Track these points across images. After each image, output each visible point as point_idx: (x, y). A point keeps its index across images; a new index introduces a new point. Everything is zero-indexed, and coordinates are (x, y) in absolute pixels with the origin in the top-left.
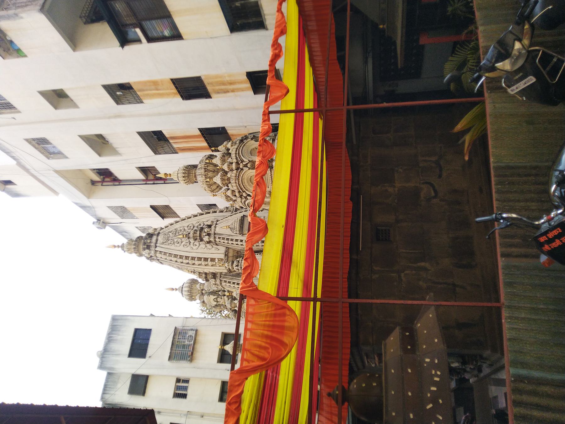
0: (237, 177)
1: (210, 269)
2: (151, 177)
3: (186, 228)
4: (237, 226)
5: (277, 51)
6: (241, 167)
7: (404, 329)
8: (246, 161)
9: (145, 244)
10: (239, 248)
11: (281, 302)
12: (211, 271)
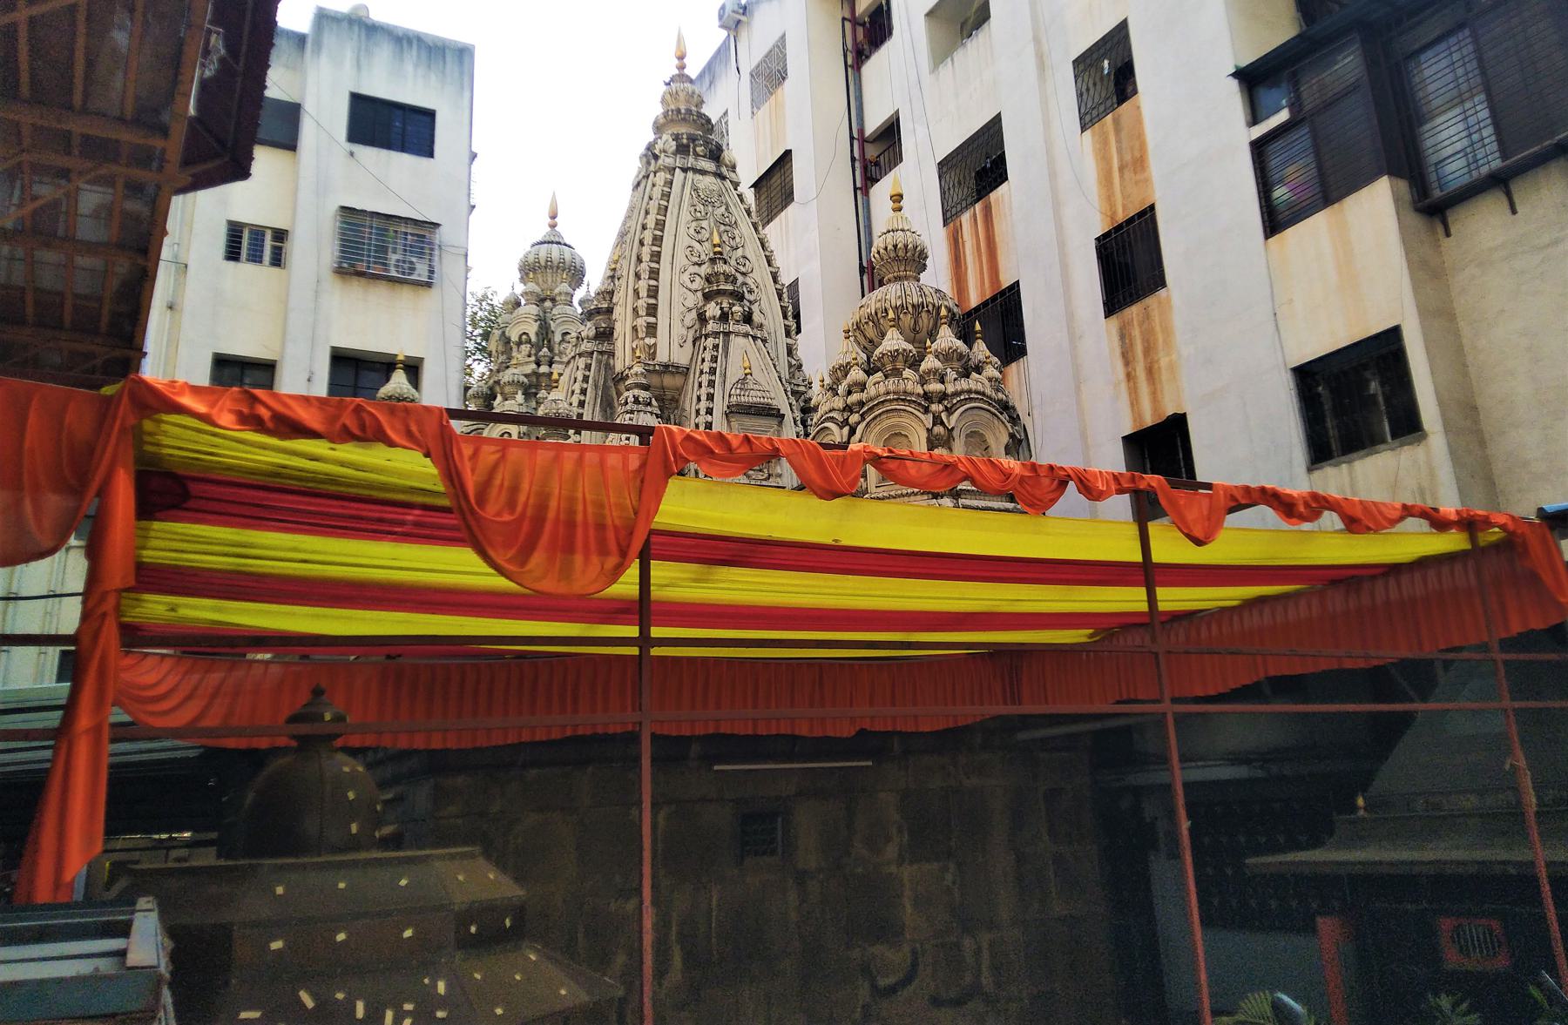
0: (903, 397)
1: (623, 322)
2: (872, 152)
3: (740, 252)
4: (753, 398)
5: (1302, 509)
6: (934, 407)
7: (519, 912)
8: (952, 421)
9: (692, 139)
10: (689, 404)
11: (637, 545)
12: (618, 327)
